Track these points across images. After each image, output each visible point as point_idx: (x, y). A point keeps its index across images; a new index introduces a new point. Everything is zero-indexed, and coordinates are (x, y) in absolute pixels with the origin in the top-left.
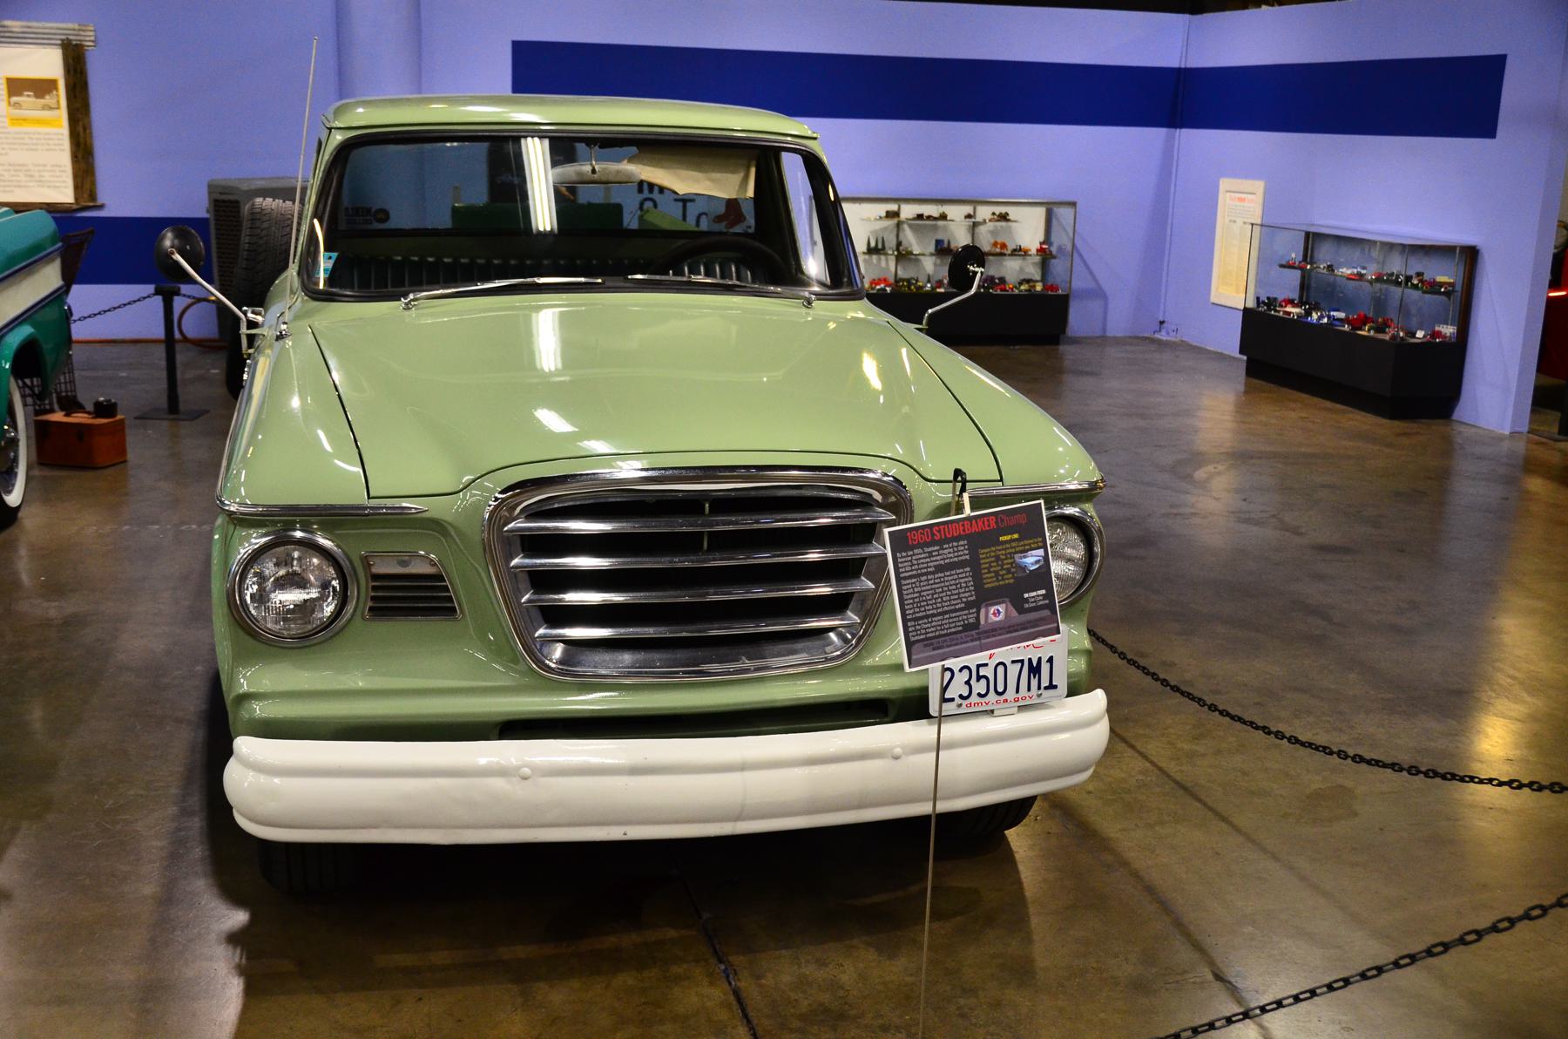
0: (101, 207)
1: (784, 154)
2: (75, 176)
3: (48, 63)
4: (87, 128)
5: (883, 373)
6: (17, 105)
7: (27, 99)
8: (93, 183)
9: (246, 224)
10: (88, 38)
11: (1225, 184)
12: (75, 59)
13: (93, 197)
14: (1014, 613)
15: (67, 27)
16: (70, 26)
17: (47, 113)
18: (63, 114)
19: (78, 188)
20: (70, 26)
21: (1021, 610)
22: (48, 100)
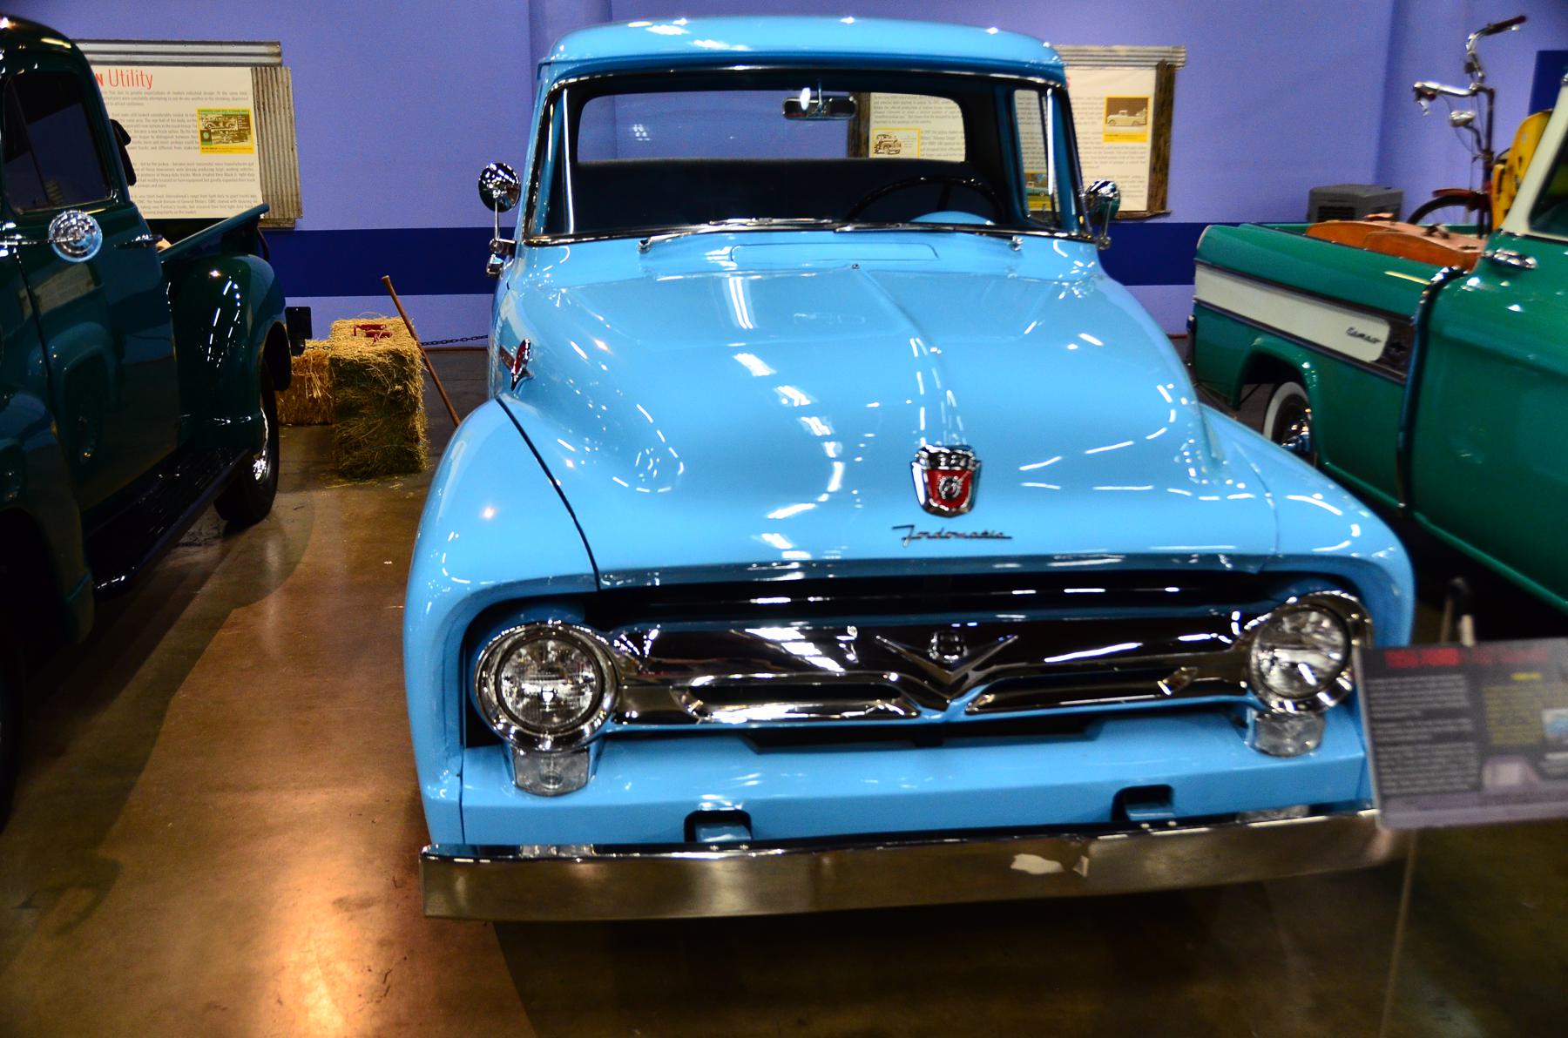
0: (1167, 214)
1: (580, 160)
2: (1151, 186)
3: (1142, 83)
4: (1167, 142)
5: (1011, 623)
6: (1112, 123)
7: (1122, 117)
8: (1165, 192)
9: (499, 323)
10: (1180, 58)
11: (962, 159)
12: (1166, 77)
13: (1163, 204)
14: (1534, 778)
15: (1160, 50)
16: (1166, 48)
17: (1136, 129)
18: (1148, 130)
19: (1152, 197)
20: (1166, 48)
21: (1544, 775)
22: (1139, 117)
